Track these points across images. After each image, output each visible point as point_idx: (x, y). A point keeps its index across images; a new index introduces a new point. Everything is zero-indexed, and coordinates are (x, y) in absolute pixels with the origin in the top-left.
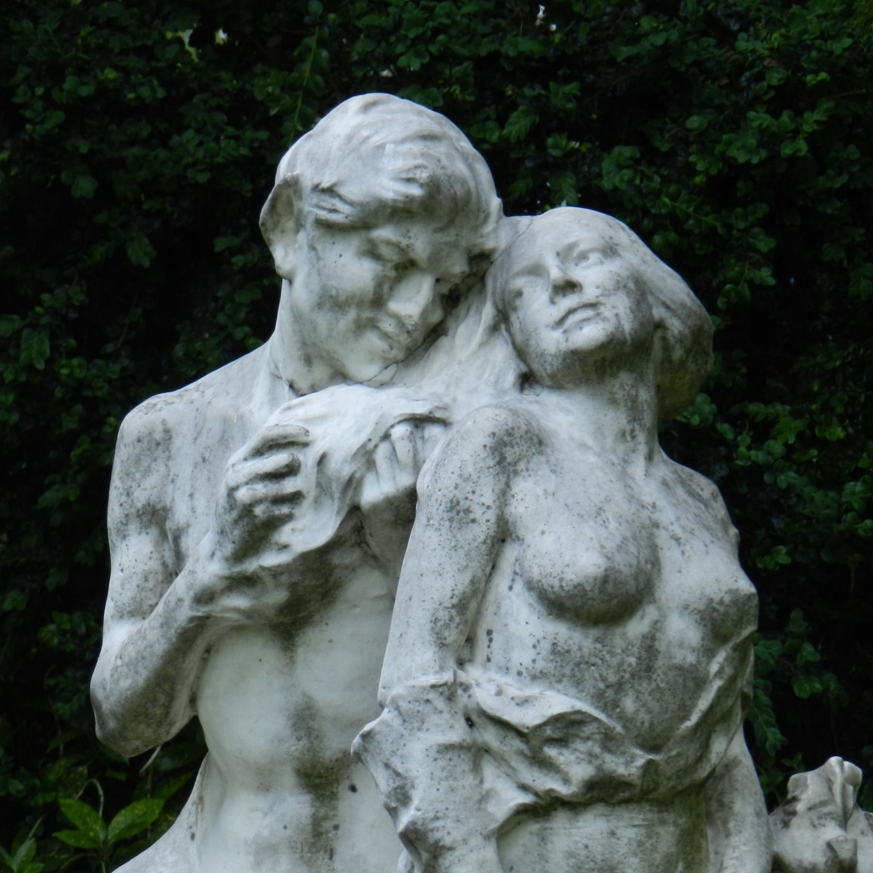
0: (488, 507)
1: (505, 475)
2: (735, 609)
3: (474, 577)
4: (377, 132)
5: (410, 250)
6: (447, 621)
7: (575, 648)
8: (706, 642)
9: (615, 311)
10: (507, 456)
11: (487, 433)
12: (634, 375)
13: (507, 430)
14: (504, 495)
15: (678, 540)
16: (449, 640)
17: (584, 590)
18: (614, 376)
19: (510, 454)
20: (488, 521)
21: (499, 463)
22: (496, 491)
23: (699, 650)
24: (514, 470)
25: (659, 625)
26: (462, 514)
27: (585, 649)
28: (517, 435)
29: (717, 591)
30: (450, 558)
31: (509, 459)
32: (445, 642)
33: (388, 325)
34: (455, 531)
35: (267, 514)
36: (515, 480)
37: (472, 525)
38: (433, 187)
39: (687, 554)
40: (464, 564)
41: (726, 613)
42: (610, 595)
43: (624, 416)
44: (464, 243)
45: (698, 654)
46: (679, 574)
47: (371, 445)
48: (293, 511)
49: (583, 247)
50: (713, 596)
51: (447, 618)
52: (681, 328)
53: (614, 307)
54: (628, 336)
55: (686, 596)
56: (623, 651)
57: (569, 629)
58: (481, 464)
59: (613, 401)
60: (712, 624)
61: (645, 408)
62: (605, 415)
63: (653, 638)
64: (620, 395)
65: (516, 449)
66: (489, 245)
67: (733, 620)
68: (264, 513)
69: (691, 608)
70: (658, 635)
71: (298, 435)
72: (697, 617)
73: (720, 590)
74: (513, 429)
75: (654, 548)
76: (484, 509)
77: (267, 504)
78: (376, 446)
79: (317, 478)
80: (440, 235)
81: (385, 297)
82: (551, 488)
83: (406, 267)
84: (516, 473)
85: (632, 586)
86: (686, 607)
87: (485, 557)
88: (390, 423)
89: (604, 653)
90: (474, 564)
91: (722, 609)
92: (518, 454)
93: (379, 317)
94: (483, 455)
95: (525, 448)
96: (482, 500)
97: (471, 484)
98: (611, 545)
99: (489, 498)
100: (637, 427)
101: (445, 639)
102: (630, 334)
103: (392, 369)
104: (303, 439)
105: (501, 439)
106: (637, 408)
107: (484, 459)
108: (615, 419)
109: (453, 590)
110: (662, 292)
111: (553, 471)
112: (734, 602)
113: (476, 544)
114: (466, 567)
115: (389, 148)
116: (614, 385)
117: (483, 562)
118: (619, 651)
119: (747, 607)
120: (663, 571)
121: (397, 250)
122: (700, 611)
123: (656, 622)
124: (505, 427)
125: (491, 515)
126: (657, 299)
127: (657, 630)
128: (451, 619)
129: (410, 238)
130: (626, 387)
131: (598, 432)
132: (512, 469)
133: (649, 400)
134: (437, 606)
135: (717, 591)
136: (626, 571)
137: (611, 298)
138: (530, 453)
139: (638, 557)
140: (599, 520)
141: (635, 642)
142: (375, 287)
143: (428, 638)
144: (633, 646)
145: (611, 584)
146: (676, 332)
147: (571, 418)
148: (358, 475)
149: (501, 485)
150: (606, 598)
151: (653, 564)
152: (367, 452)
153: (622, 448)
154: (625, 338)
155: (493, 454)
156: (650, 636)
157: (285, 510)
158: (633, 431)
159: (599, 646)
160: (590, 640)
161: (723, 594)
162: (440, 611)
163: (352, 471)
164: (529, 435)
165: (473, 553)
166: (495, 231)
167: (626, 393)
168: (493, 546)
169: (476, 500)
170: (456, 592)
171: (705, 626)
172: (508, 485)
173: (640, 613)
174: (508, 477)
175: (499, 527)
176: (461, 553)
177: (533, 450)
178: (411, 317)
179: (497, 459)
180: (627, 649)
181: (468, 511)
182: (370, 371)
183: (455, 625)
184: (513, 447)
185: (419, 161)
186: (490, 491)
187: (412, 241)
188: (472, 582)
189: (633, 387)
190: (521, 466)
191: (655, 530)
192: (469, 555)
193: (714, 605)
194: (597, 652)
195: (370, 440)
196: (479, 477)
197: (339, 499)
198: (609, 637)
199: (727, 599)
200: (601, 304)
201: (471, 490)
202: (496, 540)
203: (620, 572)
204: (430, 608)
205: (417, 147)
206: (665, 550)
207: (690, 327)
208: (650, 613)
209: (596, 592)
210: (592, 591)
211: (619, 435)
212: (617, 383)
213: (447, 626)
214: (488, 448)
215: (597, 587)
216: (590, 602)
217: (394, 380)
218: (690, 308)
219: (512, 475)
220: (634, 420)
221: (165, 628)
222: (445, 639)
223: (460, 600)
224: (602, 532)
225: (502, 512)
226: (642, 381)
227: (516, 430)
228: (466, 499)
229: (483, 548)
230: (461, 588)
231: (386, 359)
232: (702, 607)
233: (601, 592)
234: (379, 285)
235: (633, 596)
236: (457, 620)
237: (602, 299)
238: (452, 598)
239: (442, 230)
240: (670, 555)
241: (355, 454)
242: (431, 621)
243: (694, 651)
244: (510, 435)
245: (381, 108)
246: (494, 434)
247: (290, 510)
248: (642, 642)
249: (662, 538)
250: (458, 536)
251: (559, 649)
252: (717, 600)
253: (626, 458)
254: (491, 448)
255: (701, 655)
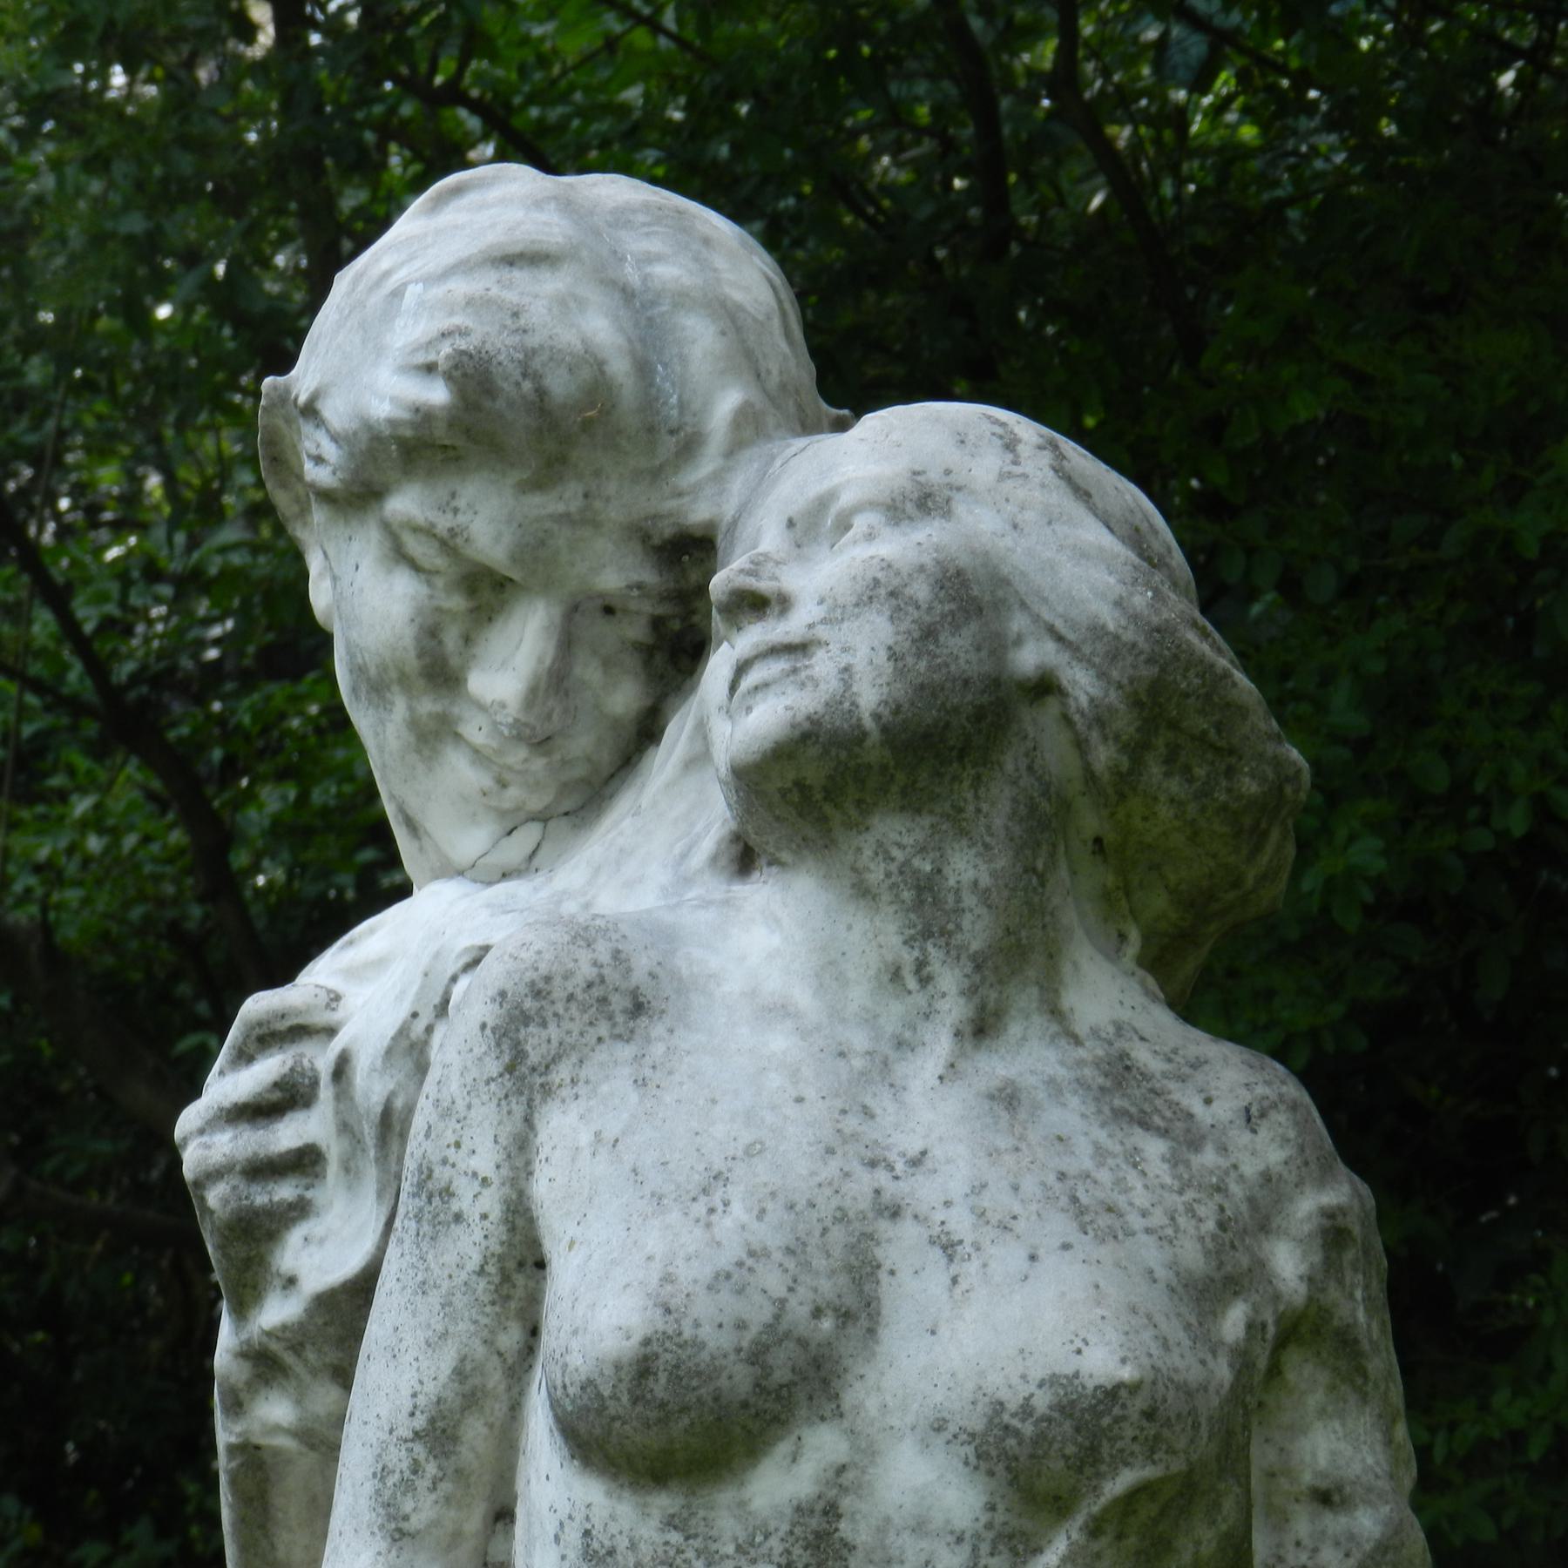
0: (485, 1182)
1: (524, 1099)
2: (1068, 1426)
3: (463, 1360)
4: (411, 258)
5: (459, 541)
6: (407, 1474)
7: (622, 1543)
8: (1000, 1517)
9: (845, 659)
10: (528, 1048)
11: (492, 992)
12: (926, 821)
13: (533, 983)
14: (521, 1149)
15: (949, 1247)
16: (415, 1523)
17: (599, 1395)
18: (858, 826)
19: (536, 1044)
20: (484, 1217)
21: (510, 1069)
22: (503, 1140)
23: (977, 1536)
24: (542, 1085)
25: (850, 1475)
26: (436, 1201)
27: (642, 1546)
28: (558, 994)
29: (1015, 1380)
30: (414, 1314)
31: (534, 1058)
32: (405, 1526)
33: (475, 730)
34: (425, 1246)
35: (233, 1205)
36: (545, 1109)
37: (457, 1230)
38: (472, 377)
39: (963, 1285)
40: (440, 1328)
41: (1040, 1439)
42: (663, 1405)
43: (892, 928)
44: (614, 514)
45: (975, 1549)
46: (929, 1338)
47: (419, 1027)
48: (309, 1194)
49: (846, 499)
50: (1004, 1395)
51: (405, 1465)
52: (1096, 691)
53: (845, 650)
54: (868, 723)
55: (939, 1397)
56: (739, 1549)
57: (609, 1494)
58: (474, 1073)
59: (863, 892)
60: (1008, 1468)
61: (969, 900)
62: (850, 928)
63: (832, 1512)
64: (876, 874)
65: (553, 1031)
66: (699, 513)
67: (1066, 1458)
68: (225, 1201)
69: (953, 1428)
70: (846, 1503)
71: (308, 1010)
72: (969, 1450)
73: (1024, 1377)
74: (548, 979)
75: (863, 1270)
76: (476, 1185)
77: (236, 1180)
78: (429, 1030)
79: (337, 1113)
80: (815, 490)
81: (454, 661)
82: (612, 1130)
83: (486, 591)
84: (547, 1091)
85: (740, 1380)
86: (939, 1427)
87: (488, 1309)
88: (449, 973)
89: (690, 1554)
90: (462, 1326)
91: (1028, 1429)
92: (555, 1043)
93: (456, 710)
94: (478, 1051)
95: (575, 1027)
96: (475, 1163)
97: (453, 1124)
98: (693, 1274)
99: (485, 1158)
100: (935, 954)
101: (406, 1518)
102: (876, 717)
103: (528, 836)
104: (321, 1018)
105: (518, 1006)
106: (936, 902)
107: (480, 1059)
108: (874, 936)
109: (414, 1395)
110: (1045, 600)
111: (641, 1083)
112: (1065, 1408)
113: (464, 1276)
114: (444, 1335)
115: (414, 291)
116: (859, 850)
117: (484, 1321)
118: (730, 1549)
119: (1106, 1421)
120: (884, 1334)
121: (437, 545)
122: (973, 1435)
123: (842, 1469)
124: (530, 975)
125: (491, 1202)
126: (1037, 618)
127: (844, 1490)
128: (416, 1468)
129: (456, 511)
130: (896, 852)
131: (829, 971)
132: (539, 1080)
133: (985, 880)
134: (385, 1436)
135: (1015, 1380)
136: (718, 1341)
137: (845, 625)
138: (592, 1035)
139: (783, 1302)
140: (699, 1209)
141: (772, 1525)
142: (417, 639)
143: (368, 1516)
144: (767, 1536)
145: (663, 1378)
146: (1084, 701)
147: (776, 940)
148: (399, 1103)
149: (515, 1124)
150: (653, 1415)
151: (845, 1317)
152: (412, 1046)
153: (894, 1012)
154: (859, 726)
155: (498, 1045)
156: (819, 1506)
157: (285, 1191)
158: (921, 965)
159: (675, 1537)
160: (654, 1523)
161: (1032, 1388)
162: (392, 1448)
163: (385, 1094)
164: (596, 992)
165: (460, 1301)
166: (718, 477)
167: (893, 867)
168: (506, 1278)
169: (462, 1166)
170: (422, 1401)
171: (991, 1473)
172: (528, 1121)
173: (783, 1448)
174: (530, 1104)
175: (512, 1229)
176: (435, 1299)
177: (603, 1029)
178: (503, 706)
179: (507, 1058)
180: (752, 1544)
181: (447, 1193)
182: (471, 842)
183: (427, 1483)
184: (544, 1024)
185: (457, 320)
186: (489, 1143)
187: (461, 519)
188: (459, 1373)
189: (922, 850)
190: (562, 1072)
191: (884, 1226)
192: (450, 1304)
193: (1006, 1418)
194: (672, 1553)
195: (415, 1015)
196: (469, 1107)
197: (377, 1160)
198: (701, 1513)
199: (1042, 1402)
200: (819, 643)
201: (451, 1139)
202: (511, 1265)
203: (699, 1345)
204: (374, 1441)
205: (485, 283)
206: (904, 1275)
207: (1120, 686)
208: (822, 1445)
209: (625, 1399)
210: (614, 1397)
211: (886, 978)
212: (868, 843)
213: (407, 1486)
214: (488, 1031)
215: (623, 1387)
216: (617, 1424)
217: (536, 862)
218: (1117, 637)
219: (538, 1098)
220: (927, 934)
221: (783, 1417)
222: (406, 1518)
223: (432, 1421)
224: (692, 1238)
225: (521, 1194)
226: (963, 833)
227: (557, 981)
228: (444, 1162)
229: (482, 1285)
230: (431, 1388)
231: (502, 814)
232: (978, 1425)
233: (635, 1401)
234: (430, 632)
235: (745, 1405)
236: (431, 1469)
237: (822, 632)
238: (412, 1414)
239: (536, 484)
240: (913, 1285)
241: (389, 1052)
242: (375, 1475)
243: (960, 1540)
244: (537, 994)
245: (472, 198)
246: (503, 994)
247: (299, 1191)
248: (794, 1525)
249: (902, 1247)
250: (430, 1257)
251: (595, 1545)
252: (1013, 1406)
253: (908, 1034)
254: (494, 1030)
255: (985, 1548)
